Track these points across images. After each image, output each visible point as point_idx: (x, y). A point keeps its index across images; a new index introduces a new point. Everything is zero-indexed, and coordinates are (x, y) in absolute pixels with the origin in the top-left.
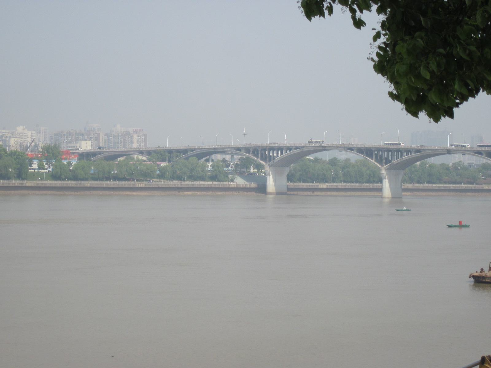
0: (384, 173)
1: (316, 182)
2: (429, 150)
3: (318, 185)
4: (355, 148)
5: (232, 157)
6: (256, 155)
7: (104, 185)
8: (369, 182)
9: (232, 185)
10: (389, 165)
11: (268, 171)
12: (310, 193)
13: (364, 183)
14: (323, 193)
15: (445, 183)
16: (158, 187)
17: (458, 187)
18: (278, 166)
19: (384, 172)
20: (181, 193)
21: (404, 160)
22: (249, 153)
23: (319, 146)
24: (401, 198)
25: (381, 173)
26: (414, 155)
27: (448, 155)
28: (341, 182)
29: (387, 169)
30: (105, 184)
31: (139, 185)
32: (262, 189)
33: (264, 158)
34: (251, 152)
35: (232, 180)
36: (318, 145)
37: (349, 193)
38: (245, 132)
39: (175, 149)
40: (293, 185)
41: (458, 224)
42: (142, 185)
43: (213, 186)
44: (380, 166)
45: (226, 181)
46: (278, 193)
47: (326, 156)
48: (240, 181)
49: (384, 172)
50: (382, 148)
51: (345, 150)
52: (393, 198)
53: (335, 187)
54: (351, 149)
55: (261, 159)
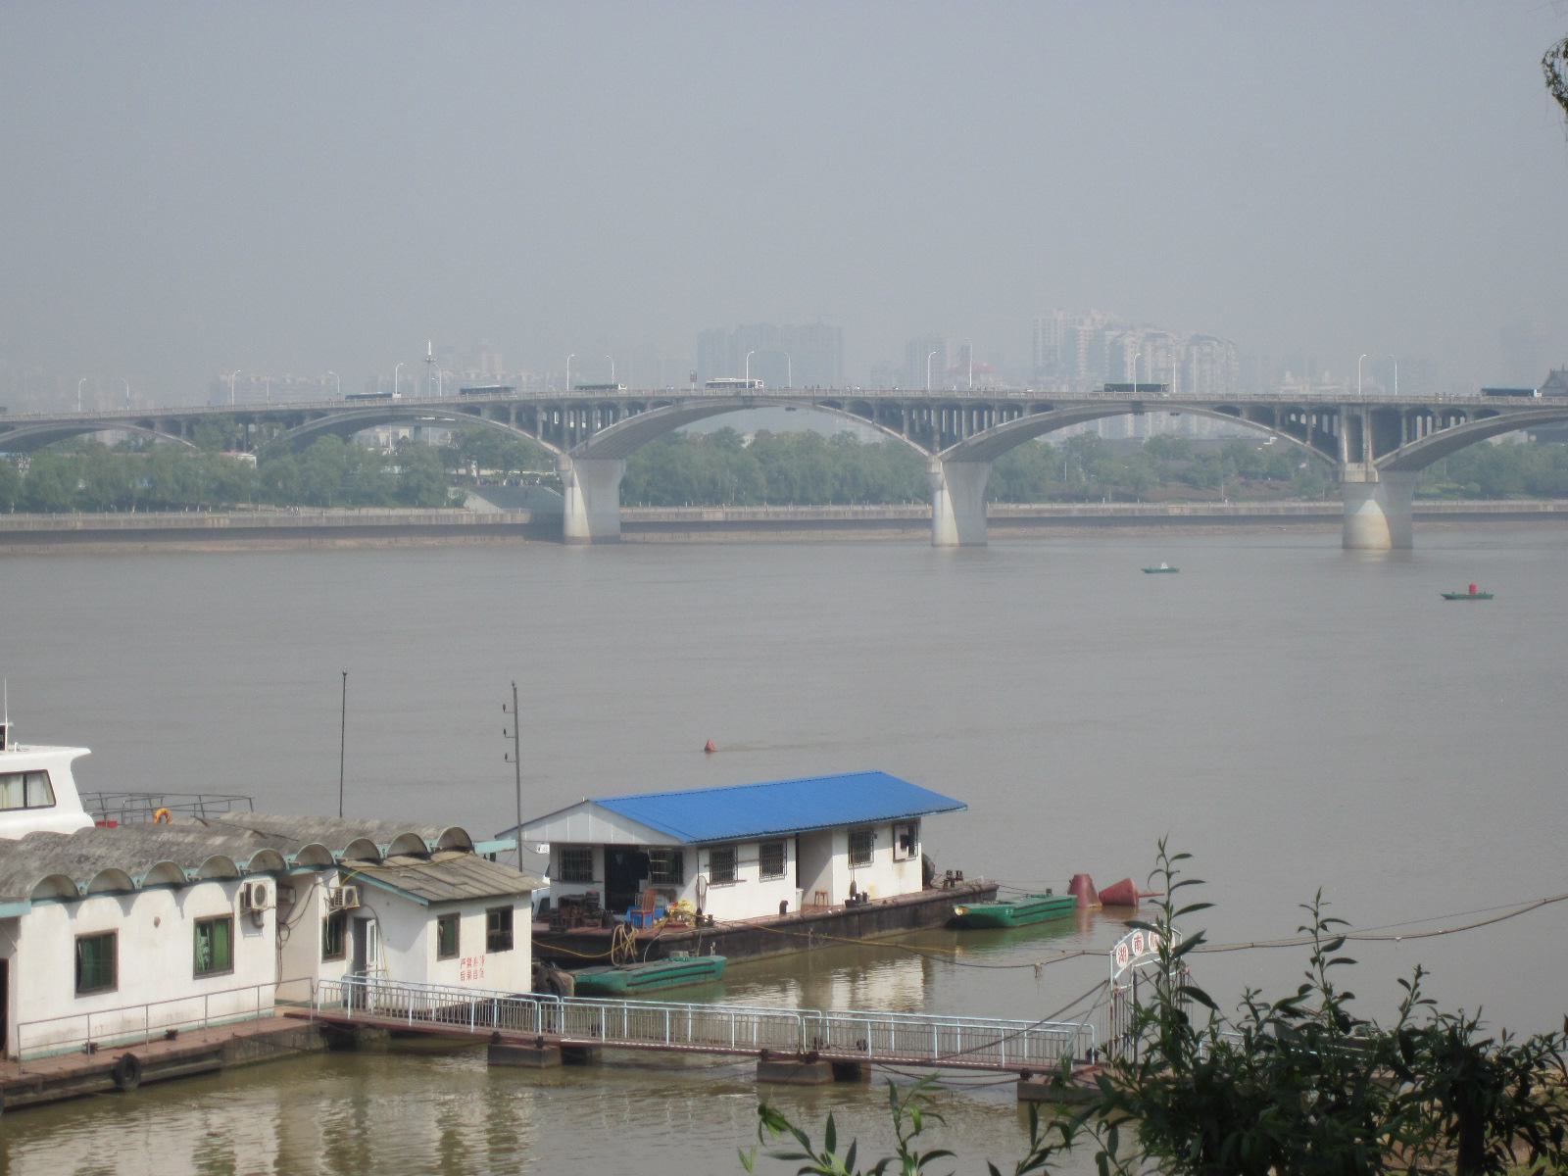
0: (939, 473)
1: (689, 504)
2: (1078, 402)
3: (701, 514)
4: (846, 402)
5: (415, 433)
6: (531, 426)
7: (122, 524)
8: (839, 499)
9: (465, 518)
10: (953, 450)
11: (570, 473)
12: (681, 537)
13: (824, 501)
14: (718, 536)
15: (1052, 499)
16: (266, 528)
17: (1092, 510)
18: (595, 459)
19: (937, 471)
20: (328, 542)
21: (999, 432)
22: (506, 420)
23: (732, 395)
24: (985, 544)
25: (932, 474)
26: (1028, 418)
27: (745, 412)
28: (760, 500)
29: (947, 462)
30: (125, 521)
31: (216, 521)
32: (549, 527)
33: (556, 435)
34: (513, 418)
35: (458, 504)
36: (729, 392)
37: (787, 535)
38: (430, 354)
39: (261, 412)
40: (1305, 508)
41: (1467, 593)
42: (222, 521)
43: (412, 521)
44: (926, 453)
45: (442, 507)
46: (599, 540)
47: (747, 426)
48: (478, 507)
49: (938, 468)
50: (933, 399)
51: (814, 407)
52: (961, 545)
53: (750, 518)
54: (833, 403)
55: (544, 438)
